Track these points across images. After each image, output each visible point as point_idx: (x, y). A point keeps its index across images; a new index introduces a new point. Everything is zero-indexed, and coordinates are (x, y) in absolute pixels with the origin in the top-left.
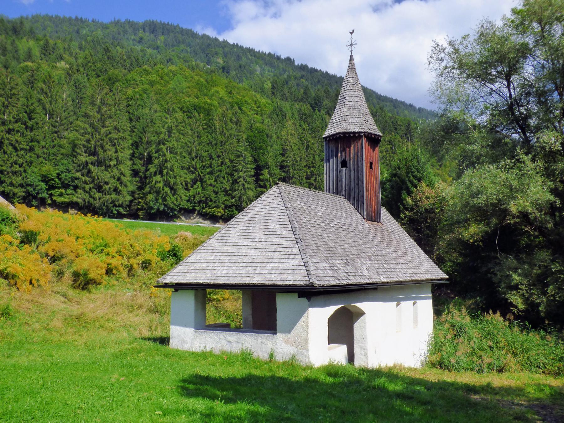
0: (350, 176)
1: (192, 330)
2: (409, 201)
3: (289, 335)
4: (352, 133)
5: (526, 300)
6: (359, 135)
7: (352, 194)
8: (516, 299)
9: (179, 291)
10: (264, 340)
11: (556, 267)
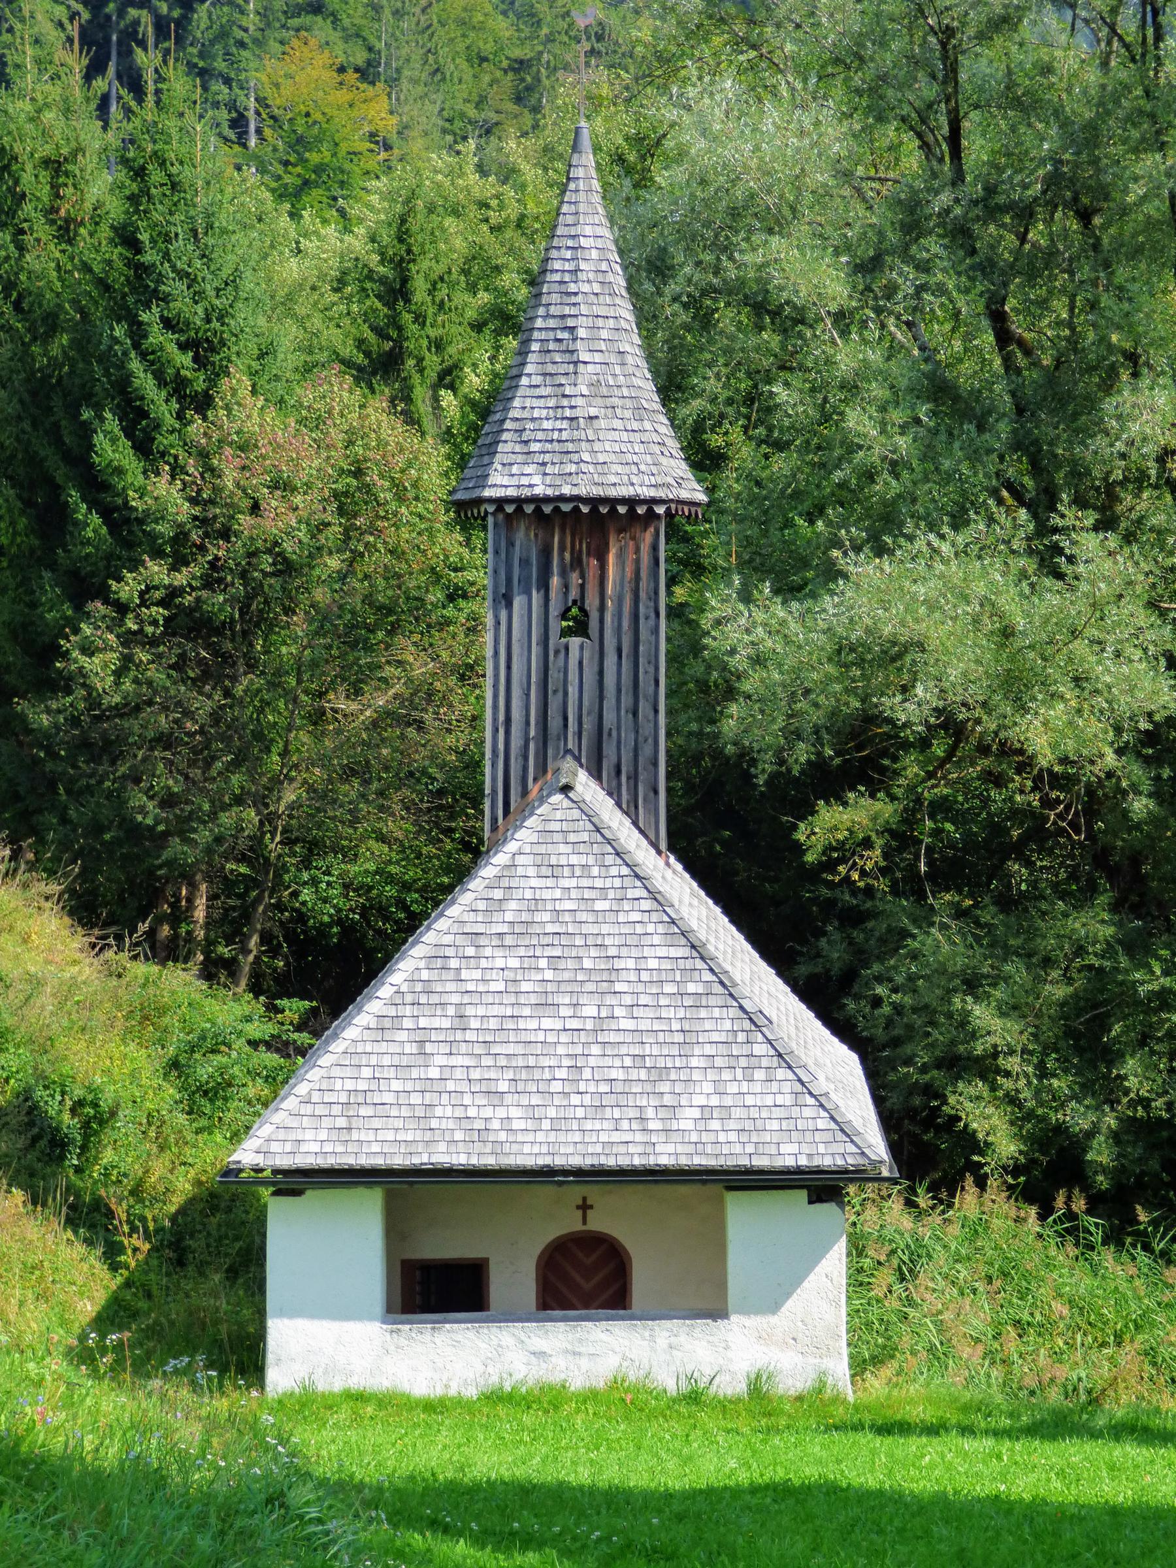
0: (601, 673)
1: (378, 1324)
2: (164, 497)
3: (773, 1319)
4: (624, 501)
5: (1021, 1116)
6: (650, 511)
7: (609, 751)
8: (988, 1117)
9: (309, 1193)
10: (683, 1338)
11: (1150, 980)
